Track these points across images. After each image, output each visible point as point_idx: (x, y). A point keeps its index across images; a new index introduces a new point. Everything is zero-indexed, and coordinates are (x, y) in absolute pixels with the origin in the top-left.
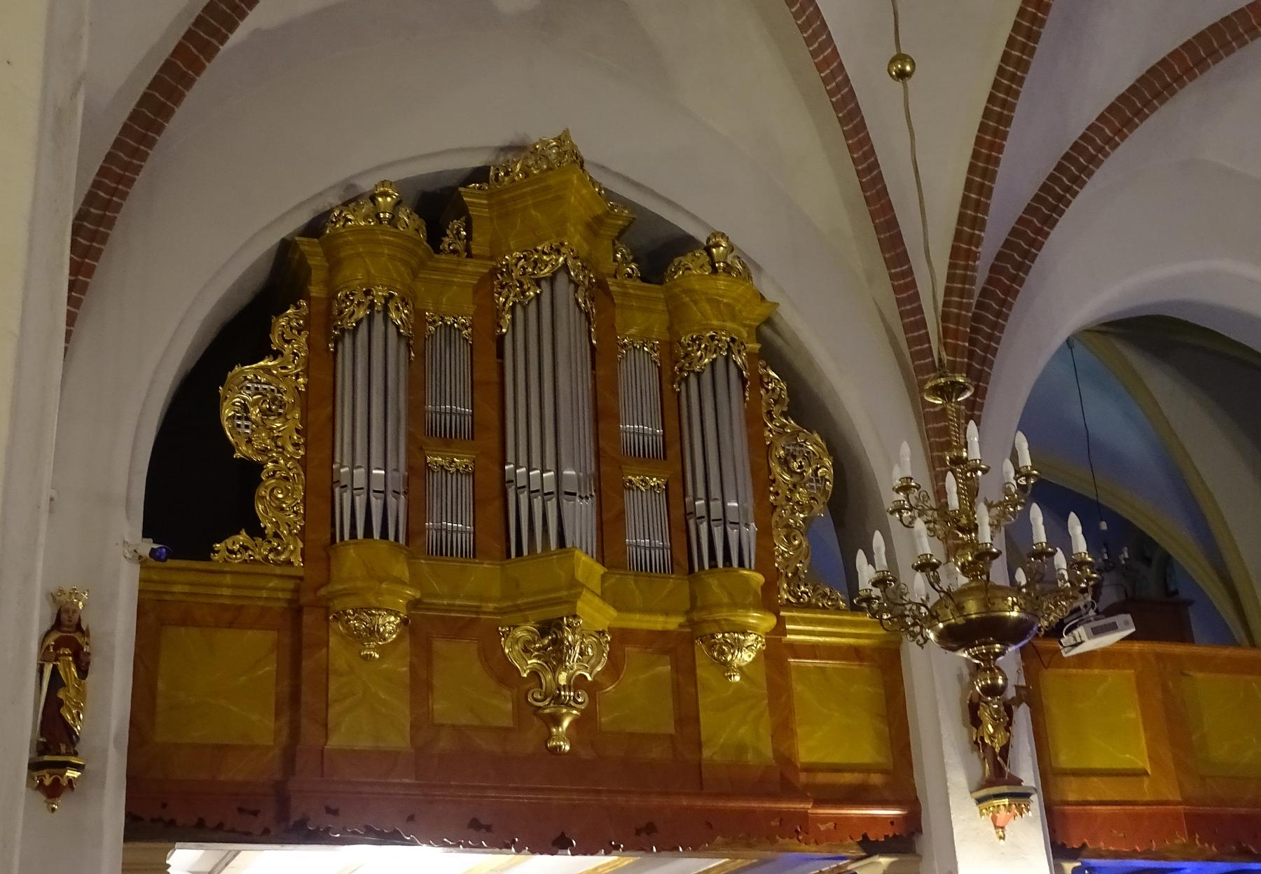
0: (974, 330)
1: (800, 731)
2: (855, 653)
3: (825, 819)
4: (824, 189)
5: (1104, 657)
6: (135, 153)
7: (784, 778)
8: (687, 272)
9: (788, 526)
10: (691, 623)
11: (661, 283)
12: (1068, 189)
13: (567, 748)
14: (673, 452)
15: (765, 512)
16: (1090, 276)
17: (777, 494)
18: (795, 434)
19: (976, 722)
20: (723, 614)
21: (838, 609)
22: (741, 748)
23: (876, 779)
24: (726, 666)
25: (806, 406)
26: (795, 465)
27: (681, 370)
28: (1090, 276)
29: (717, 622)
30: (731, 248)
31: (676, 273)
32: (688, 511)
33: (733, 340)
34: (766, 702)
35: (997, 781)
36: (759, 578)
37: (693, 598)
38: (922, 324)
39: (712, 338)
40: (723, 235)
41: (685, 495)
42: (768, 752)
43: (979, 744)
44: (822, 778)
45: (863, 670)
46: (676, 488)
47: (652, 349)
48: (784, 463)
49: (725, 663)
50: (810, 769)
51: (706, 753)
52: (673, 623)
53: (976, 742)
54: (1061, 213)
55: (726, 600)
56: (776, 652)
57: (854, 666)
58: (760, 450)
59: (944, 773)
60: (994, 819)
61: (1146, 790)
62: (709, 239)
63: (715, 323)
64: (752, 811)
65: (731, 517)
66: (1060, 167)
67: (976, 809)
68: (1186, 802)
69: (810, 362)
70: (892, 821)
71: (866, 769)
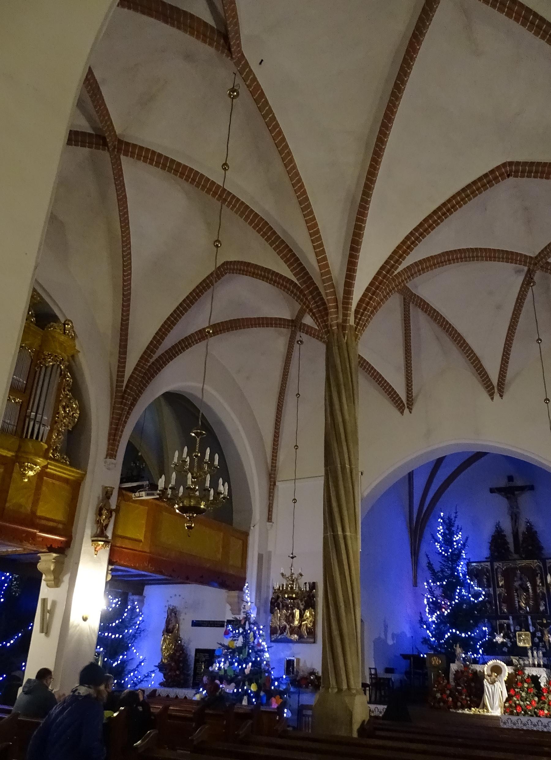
0: (140, 385)
1: (41, 503)
2: (66, 481)
3: (41, 537)
4: (107, 319)
5: (142, 502)
6: (152, 160)
7: (32, 520)
8: (55, 330)
9: (59, 430)
10: (16, 456)
11: (43, 329)
12: (180, 350)
13: (296, 636)
14: (28, 392)
15: (54, 422)
16: (174, 378)
17: (58, 418)
18: (70, 399)
19: (100, 514)
20: (31, 457)
21: (66, 464)
22: (21, 506)
23: (60, 526)
24: (24, 475)
25: (76, 391)
26: (68, 409)
27: (41, 363)
28: (174, 378)
29: (27, 458)
30: (72, 327)
31: (50, 328)
32: (27, 414)
33: (63, 359)
34: (33, 491)
35: (100, 535)
36: (46, 446)
37: (20, 447)
38: (123, 376)
39: (56, 356)
40: (72, 323)
41: (28, 408)
42: (29, 509)
43: (98, 522)
44: (43, 522)
45: (67, 487)
46: (25, 404)
47: (32, 351)
48: (64, 408)
49: (25, 474)
50: (41, 518)
51: (7, 505)
52: (10, 454)
53: (98, 521)
54: (175, 357)
55: (33, 451)
56: (41, 475)
57: (64, 485)
58: (58, 401)
59: (85, 529)
60: (95, 548)
61: (139, 547)
62: (65, 322)
63: (59, 351)
64: (17, 530)
65: (43, 422)
66: (179, 342)
67: (91, 543)
68: (150, 553)
69: (83, 375)
70: (61, 542)
71: (58, 522)
